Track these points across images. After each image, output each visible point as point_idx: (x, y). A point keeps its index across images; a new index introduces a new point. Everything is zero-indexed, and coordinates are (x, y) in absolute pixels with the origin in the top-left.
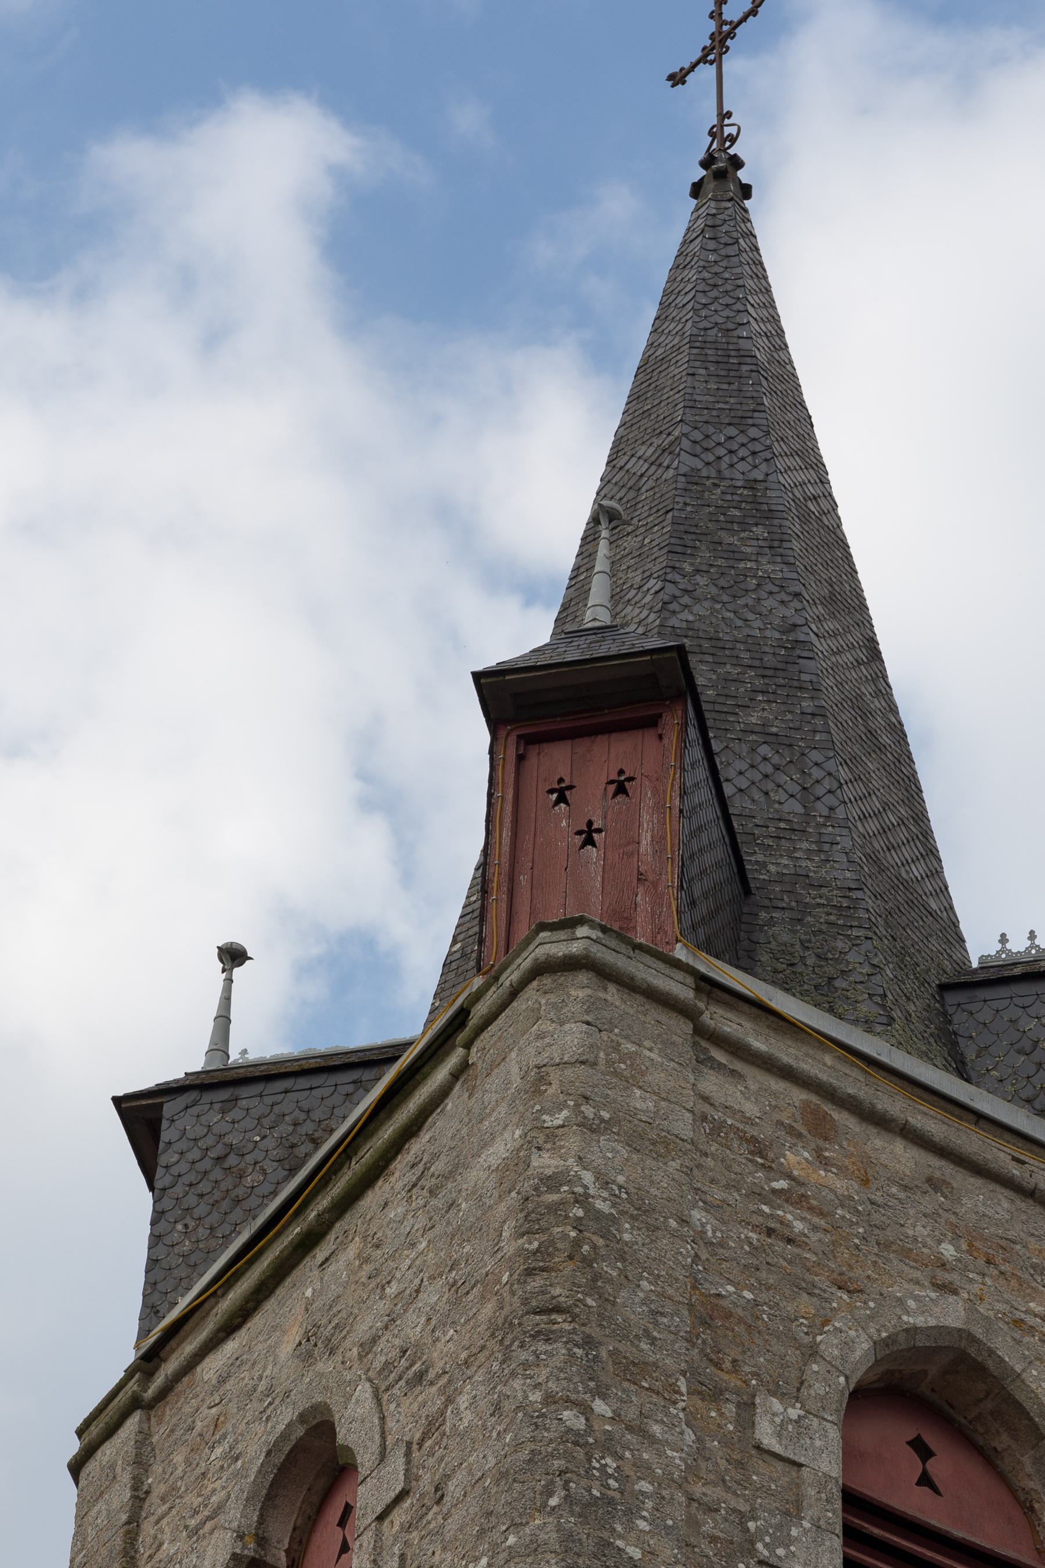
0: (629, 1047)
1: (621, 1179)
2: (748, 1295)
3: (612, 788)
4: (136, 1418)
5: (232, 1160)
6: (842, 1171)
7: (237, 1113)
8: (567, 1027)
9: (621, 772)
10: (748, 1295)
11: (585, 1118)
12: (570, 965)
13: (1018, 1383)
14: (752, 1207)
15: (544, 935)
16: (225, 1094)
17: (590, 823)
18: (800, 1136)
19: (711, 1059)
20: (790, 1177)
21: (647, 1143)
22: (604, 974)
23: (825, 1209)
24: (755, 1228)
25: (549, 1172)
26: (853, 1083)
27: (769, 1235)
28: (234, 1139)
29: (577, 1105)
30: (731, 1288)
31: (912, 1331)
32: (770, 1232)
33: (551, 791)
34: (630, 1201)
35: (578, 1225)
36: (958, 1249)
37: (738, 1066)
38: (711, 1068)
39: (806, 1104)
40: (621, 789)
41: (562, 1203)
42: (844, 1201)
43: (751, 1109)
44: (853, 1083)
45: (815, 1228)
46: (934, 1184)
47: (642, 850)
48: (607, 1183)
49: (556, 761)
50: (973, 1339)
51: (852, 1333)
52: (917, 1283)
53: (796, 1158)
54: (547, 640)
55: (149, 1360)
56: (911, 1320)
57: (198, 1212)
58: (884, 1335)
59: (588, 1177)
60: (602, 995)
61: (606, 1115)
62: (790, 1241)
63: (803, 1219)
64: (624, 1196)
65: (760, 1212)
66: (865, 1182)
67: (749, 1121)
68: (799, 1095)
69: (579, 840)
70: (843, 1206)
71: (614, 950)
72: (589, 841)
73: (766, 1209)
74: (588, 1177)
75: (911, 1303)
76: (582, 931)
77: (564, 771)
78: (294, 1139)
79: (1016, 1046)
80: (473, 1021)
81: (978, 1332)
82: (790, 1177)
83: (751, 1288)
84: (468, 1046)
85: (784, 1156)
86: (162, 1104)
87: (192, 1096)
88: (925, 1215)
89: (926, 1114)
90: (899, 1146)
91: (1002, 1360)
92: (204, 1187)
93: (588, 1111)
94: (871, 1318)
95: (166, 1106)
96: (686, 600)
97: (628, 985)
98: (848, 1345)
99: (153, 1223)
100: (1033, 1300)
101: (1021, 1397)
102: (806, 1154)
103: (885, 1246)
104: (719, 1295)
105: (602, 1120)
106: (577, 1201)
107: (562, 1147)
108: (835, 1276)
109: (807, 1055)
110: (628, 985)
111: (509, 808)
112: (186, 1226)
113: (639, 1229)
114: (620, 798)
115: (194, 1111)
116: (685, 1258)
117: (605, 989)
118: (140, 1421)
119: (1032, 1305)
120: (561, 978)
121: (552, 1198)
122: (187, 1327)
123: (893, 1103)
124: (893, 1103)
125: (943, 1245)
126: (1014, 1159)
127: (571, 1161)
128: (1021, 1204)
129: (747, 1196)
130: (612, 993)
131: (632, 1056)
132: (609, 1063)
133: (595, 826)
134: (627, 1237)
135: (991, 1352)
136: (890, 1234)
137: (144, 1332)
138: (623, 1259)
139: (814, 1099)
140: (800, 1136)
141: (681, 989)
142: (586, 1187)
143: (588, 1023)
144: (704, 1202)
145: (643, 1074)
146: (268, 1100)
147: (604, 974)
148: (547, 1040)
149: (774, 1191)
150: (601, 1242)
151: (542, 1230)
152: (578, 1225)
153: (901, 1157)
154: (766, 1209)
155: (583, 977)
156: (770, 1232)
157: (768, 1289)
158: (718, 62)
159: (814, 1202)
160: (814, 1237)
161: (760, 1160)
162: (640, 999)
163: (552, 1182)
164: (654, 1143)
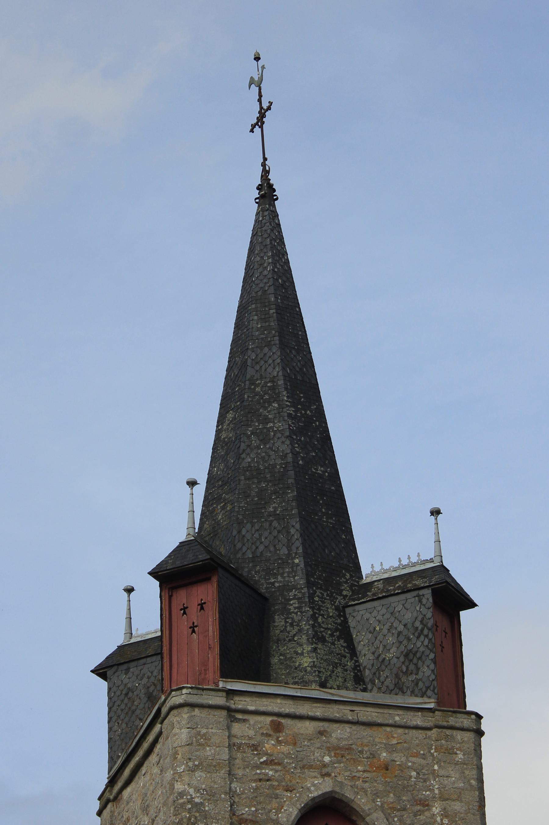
0: (204, 731)
1: (204, 786)
2: (253, 809)
3: (199, 607)
4: (109, 806)
5: (130, 694)
6: (287, 743)
7: (130, 675)
8: (182, 731)
9: (202, 600)
10: (253, 809)
11: (190, 767)
12: (181, 706)
13: (353, 803)
14: (254, 773)
15: (173, 693)
16: (125, 667)
17: (193, 623)
18: (270, 735)
19: (237, 718)
20: (267, 754)
21: (212, 767)
22: (193, 706)
23: (280, 762)
24: (255, 781)
25: (180, 791)
26: (288, 707)
27: (260, 782)
28: (129, 685)
29: (187, 763)
30: (247, 809)
31: (314, 798)
32: (260, 780)
33: (181, 610)
34: (207, 794)
35: (189, 811)
36: (330, 757)
37: (246, 717)
38: (237, 722)
39: (272, 721)
40: (202, 608)
41: (184, 803)
42: (288, 756)
43: (251, 733)
44: (288, 707)
45: (276, 771)
46: (321, 733)
47: (210, 634)
48: (199, 790)
49: (181, 597)
50: (336, 792)
51: (291, 810)
52: (315, 777)
53: (269, 745)
54: (158, 583)
55: (112, 782)
56: (312, 795)
57: (122, 717)
58: (302, 805)
59: (192, 791)
60: (193, 714)
61: (197, 763)
62: (268, 780)
63: (271, 770)
64: (205, 793)
65: (257, 773)
66: (295, 744)
67: (250, 738)
68: (269, 719)
69: (191, 630)
70: (287, 758)
71: (196, 695)
72: (194, 631)
73: (258, 771)
74: (192, 791)
75: (312, 788)
76: (184, 691)
77: (184, 601)
78: (148, 685)
79: (369, 630)
80: (163, 715)
81: (337, 789)
82: (267, 754)
83: (254, 806)
84: (162, 723)
85: (265, 747)
86: (106, 672)
87: (116, 667)
88: (318, 748)
89: (316, 707)
90: (307, 723)
91: (347, 797)
92: (123, 706)
93: (190, 764)
94: (297, 801)
95: (108, 673)
96: (248, 450)
97: (201, 706)
98: (289, 815)
99: (109, 722)
100: (359, 765)
101: (355, 807)
102: (273, 742)
103: (303, 767)
104: (243, 814)
105: (196, 765)
106: (188, 802)
107: (183, 780)
108: (285, 787)
109: (271, 702)
110: (201, 706)
111: (167, 621)
112: (118, 723)
113: (211, 804)
114: (202, 611)
115: (116, 674)
116: (228, 808)
117: (194, 710)
118: (111, 807)
119: (359, 768)
120: (179, 710)
121: (181, 801)
122: (118, 776)
123: (304, 709)
124: (304, 709)
125: (325, 757)
126: (351, 711)
127: (186, 787)
128: (354, 727)
129: (251, 769)
130: (197, 711)
131: (205, 734)
132: (197, 741)
133: (195, 625)
134: (207, 808)
135: (343, 795)
136: (305, 762)
137: (110, 769)
138: (206, 818)
139: (275, 718)
140: (270, 735)
141: (220, 700)
142: (191, 795)
143: (188, 728)
144: (236, 778)
145: (210, 740)
146: (139, 668)
147: (193, 706)
148: (177, 737)
149: (261, 763)
150: (198, 814)
151: (179, 814)
152: (189, 811)
153: (309, 727)
154: (258, 771)
155: (186, 709)
156: (260, 780)
157: (260, 803)
158: (261, 127)
159: (276, 761)
160: (277, 775)
161: (256, 753)
162: (207, 710)
163: (181, 794)
164: (215, 766)
